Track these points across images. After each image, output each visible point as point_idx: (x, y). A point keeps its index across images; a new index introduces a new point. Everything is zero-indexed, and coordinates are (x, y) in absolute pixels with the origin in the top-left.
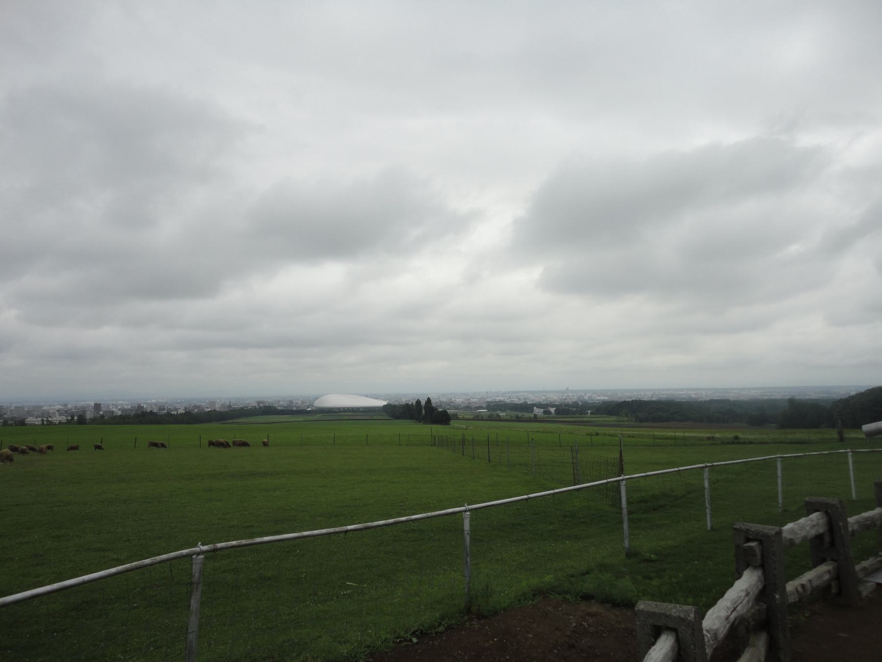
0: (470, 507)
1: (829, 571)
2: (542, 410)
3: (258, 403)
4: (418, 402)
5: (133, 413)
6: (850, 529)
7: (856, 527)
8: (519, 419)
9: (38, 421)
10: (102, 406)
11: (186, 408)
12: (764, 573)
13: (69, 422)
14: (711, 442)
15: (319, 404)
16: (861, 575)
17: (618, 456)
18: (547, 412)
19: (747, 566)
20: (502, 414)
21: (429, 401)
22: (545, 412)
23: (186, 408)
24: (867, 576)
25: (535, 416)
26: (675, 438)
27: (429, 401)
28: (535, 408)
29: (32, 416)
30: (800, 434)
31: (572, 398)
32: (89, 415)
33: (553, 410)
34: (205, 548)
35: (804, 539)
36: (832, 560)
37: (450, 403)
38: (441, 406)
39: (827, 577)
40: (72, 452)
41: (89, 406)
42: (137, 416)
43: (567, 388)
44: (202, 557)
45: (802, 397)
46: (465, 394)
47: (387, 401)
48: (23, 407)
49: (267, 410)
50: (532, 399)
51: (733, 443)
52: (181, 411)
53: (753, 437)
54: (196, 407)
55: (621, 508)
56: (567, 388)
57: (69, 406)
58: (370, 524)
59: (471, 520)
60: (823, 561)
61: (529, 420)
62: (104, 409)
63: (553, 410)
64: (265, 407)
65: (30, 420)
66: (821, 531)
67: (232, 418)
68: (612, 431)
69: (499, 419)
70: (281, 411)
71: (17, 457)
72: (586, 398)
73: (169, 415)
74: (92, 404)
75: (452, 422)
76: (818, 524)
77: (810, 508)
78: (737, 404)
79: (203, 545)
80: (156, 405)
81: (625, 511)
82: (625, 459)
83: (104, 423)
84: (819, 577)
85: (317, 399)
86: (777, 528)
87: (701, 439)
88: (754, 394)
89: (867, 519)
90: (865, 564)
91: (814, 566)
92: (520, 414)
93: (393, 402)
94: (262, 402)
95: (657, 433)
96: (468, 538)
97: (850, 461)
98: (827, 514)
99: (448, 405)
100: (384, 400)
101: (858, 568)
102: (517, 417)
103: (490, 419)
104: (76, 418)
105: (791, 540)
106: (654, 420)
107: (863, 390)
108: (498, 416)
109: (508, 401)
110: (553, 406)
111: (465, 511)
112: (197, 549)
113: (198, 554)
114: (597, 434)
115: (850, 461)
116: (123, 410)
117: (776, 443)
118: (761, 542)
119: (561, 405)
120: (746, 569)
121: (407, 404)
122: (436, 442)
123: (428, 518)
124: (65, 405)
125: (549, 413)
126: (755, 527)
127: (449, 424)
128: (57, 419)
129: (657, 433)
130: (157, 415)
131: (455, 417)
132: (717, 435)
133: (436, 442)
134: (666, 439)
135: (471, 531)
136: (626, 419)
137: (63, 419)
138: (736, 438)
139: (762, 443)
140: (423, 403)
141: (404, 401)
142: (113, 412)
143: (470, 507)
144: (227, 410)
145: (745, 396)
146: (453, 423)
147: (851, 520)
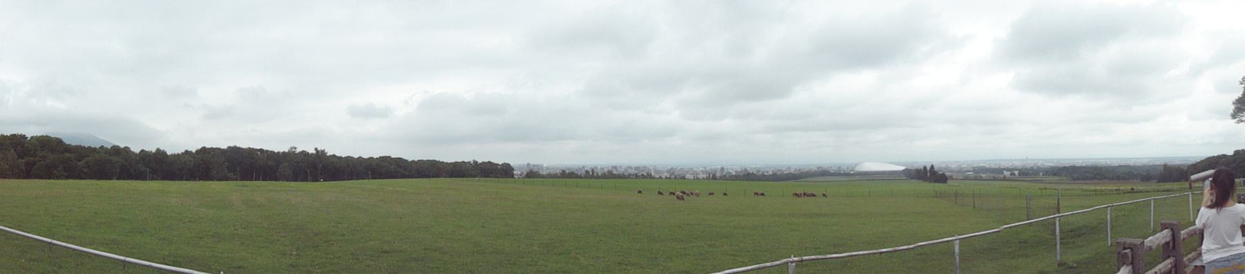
0: (959, 237)
1: (1171, 263)
2: (1009, 173)
3: (818, 168)
4: (925, 168)
5: (742, 174)
6: (1182, 238)
7: (1185, 236)
8: (995, 179)
9: (691, 177)
11: (773, 172)
12: (1133, 268)
13: (708, 178)
14: (1117, 192)
16: (1187, 263)
17: (1057, 202)
18: (1013, 174)
19: (1124, 264)
20: (983, 176)
21: (932, 167)
22: (1011, 174)
23: (773, 172)
24: (1190, 262)
25: (1005, 176)
26: (1096, 191)
27: (932, 167)
28: (1005, 171)
29: (688, 173)
30: (1168, 186)
31: (1030, 164)
32: (718, 175)
33: (1016, 173)
34: (796, 259)
35: (1158, 246)
36: (1173, 256)
37: (947, 168)
38: (940, 170)
39: (1170, 266)
40: (711, 196)
41: (718, 169)
42: (744, 176)
43: (1027, 158)
44: (794, 264)
45: (1171, 164)
46: (958, 162)
48: (683, 169)
49: (824, 173)
50: (1004, 165)
51: (1130, 192)
52: (771, 173)
53: (1141, 188)
54: (779, 170)
55: (1056, 236)
56: (1027, 158)
57: (708, 169)
58: (897, 248)
59: (960, 246)
60: (1169, 257)
61: (1001, 180)
62: (726, 171)
63: (1016, 173)
64: (823, 171)
65: (688, 176)
66: (1168, 240)
68: (1056, 186)
69: (981, 179)
71: (685, 196)
72: (1039, 164)
73: (763, 175)
74: (720, 167)
75: (949, 181)
76: (1166, 236)
77: (1164, 227)
78: (1134, 167)
79: (794, 257)
80: (755, 168)
81: (1058, 238)
82: (1061, 205)
83: (727, 180)
84: (1165, 267)
86: (1142, 240)
87: (1110, 190)
88: (1145, 162)
89: (1192, 230)
90: (1190, 256)
91: (1163, 261)
92: (996, 175)
93: (909, 167)
94: (821, 168)
95: (1085, 187)
96: (957, 257)
97: (1191, 199)
98: (1172, 229)
100: (903, 166)
101: (1185, 259)
102: (994, 177)
103: (975, 179)
104: (711, 176)
105: (1150, 247)
106: (1084, 179)
107: (1203, 159)
108: (981, 177)
109: (988, 166)
110: (1017, 170)
111: (956, 240)
112: (791, 260)
113: (792, 262)
114: (1046, 189)
115: (1191, 199)
116: (736, 172)
117: (1155, 191)
118: (1132, 249)
119: (1022, 169)
120: (1122, 266)
121: (918, 170)
122: (938, 195)
123: (930, 244)
124: (705, 168)
125: (1014, 174)
126: (1129, 240)
128: (701, 176)
129: (1085, 187)
131: (951, 178)
132: (1122, 188)
133: (938, 195)
134: (1090, 191)
135: (960, 254)
136: (1065, 178)
137: (705, 176)
138: (1132, 189)
139: (1147, 192)
140: (928, 168)
141: (916, 166)
142: (731, 173)
143: (959, 237)
144: (798, 172)
145: (1139, 163)
146: (950, 182)
147: (1183, 232)
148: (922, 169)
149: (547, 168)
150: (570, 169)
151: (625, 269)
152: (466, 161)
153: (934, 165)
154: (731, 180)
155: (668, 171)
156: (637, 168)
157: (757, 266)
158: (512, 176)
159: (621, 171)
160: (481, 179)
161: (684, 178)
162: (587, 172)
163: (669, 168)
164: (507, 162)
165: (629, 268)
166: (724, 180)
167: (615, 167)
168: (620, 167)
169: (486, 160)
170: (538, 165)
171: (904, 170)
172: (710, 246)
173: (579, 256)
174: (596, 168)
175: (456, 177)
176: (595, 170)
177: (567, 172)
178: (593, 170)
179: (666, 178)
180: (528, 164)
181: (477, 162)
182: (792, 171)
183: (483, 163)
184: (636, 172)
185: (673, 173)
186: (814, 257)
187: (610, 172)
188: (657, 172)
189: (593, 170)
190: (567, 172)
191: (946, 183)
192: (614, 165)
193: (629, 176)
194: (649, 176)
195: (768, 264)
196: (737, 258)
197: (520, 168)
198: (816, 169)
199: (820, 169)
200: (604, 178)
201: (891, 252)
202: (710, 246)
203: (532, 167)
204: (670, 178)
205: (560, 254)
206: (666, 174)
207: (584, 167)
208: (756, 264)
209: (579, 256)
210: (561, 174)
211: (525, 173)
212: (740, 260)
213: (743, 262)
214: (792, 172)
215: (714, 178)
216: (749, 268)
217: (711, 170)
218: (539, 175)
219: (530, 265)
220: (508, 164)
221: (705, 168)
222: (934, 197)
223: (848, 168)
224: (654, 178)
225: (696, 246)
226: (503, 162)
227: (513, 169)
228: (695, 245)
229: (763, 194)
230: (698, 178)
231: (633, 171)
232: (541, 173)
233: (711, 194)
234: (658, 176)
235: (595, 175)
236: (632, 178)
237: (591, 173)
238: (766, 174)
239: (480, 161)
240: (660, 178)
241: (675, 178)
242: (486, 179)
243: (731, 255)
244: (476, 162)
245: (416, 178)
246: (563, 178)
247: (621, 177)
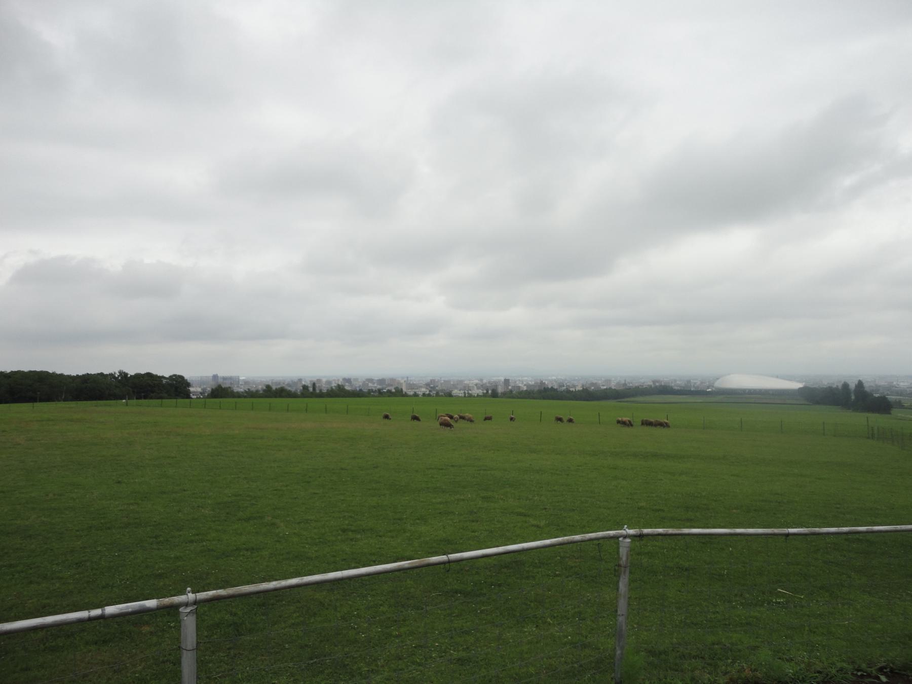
3: (654, 382)
5: (536, 389)
11: (583, 386)
13: (485, 395)
15: (720, 384)
29: (456, 388)
32: (500, 390)
34: (631, 532)
42: (540, 392)
47: (804, 384)
49: (663, 390)
52: (579, 388)
54: (593, 384)
57: (485, 381)
58: (817, 530)
62: (512, 384)
65: (455, 392)
67: (623, 397)
70: (678, 391)
73: (568, 391)
74: (502, 379)
79: (629, 528)
80: (555, 381)
83: (513, 397)
85: (718, 379)
94: (658, 381)
99: (889, 390)
104: (490, 392)
113: (625, 537)
122: (872, 435)
124: (481, 380)
127: (890, 414)
128: (476, 392)
130: (557, 391)
131: (900, 405)
137: (480, 392)
144: (622, 388)
146: (895, 412)
148: (840, 387)
149: (246, 382)
150: (279, 384)
152: (106, 372)
155: (427, 385)
156: (382, 381)
158: (187, 395)
159: (357, 385)
160: (131, 402)
161: (449, 395)
162: (305, 387)
163: (428, 379)
164: (178, 373)
165: (359, 536)
166: (509, 397)
167: (348, 380)
168: (356, 380)
169: (143, 371)
170: (231, 378)
171: (800, 389)
174: (319, 380)
175: (86, 399)
176: (317, 385)
177: (274, 388)
178: (314, 385)
179: (424, 395)
180: (215, 377)
181: (126, 374)
182: (613, 385)
183: (138, 376)
184: (379, 387)
185: (434, 388)
188: (411, 386)
189: (314, 385)
190: (274, 388)
193: (369, 394)
194: (399, 393)
197: (201, 382)
198: (651, 383)
199: (657, 384)
201: (805, 535)
203: (220, 381)
204: (429, 395)
205: (248, 520)
206: (423, 390)
207: (300, 380)
210: (264, 391)
212: (535, 522)
214: (613, 388)
215: (495, 394)
218: (232, 392)
219: (192, 542)
220: (182, 377)
221: (481, 380)
224: (406, 395)
225: (463, 500)
227: (188, 385)
228: (462, 497)
229: (570, 421)
230: (470, 396)
231: (375, 385)
232: (236, 389)
234: (412, 393)
236: (374, 396)
237: (311, 389)
238: (571, 389)
239: (131, 372)
240: (416, 395)
241: (437, 394)
243: (520, 514)
244: (124, 375)
245: (6, 402)
246: (266, 397)
247: (357, 394)
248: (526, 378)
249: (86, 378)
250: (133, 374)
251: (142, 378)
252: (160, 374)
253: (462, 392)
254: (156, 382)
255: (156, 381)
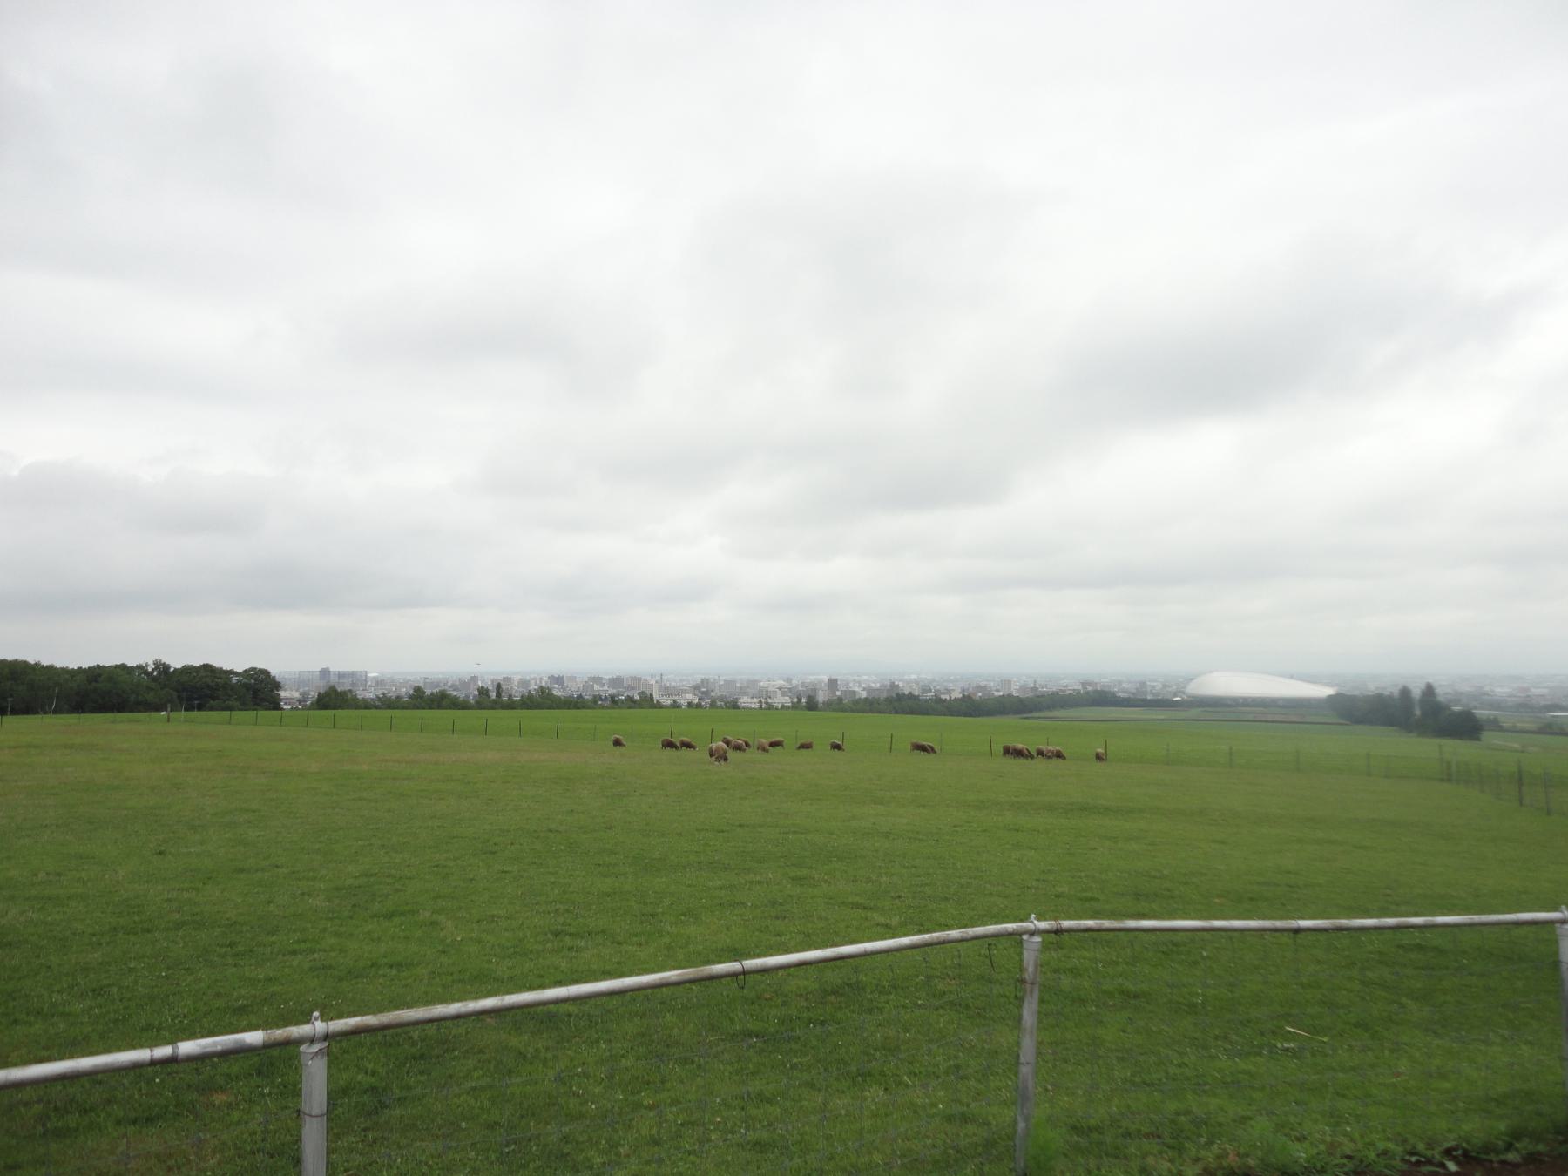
3: (1084, 684)
5: (884, 696)
9: (753, 703)
10: (839, 683)
11: (963, 690)
13: (795, 706)
29: (746, 694)
34: (1043, 925)
40: (804, 751)
42: (889, 700)
44: (1037, 939)
48: (734, 682)
49: (1100, 698)
52: (957, 695)
54: (979, 688)
57: (794, 682)
65: (744, 701)
71: (731, 754)
73: (938, 700)
74: (825, 679)
79: (1039, 920)
80: (917, 682)
83: (843, 710)
85: (1192, 679)
93: (1348, 691)
94: (1090, 684)
100: (1329, 685)
104: (804, 700)
113: (1032, 933)
116: (869, 690)
122: (1449, 775)
124: (789, 680)
128: (779, 700)
130: (919, 700)
131: (1495, 725)
137: (787, 701)
142: (854, 692)
144: (1030, 695)
146: (1488, 737)
149: (379, 683)
151: (570, 949)
152: (131, 663)
153: (1435, 685)
154: (858, 711)
155: (696, 688)
156: (617, 681)
157: (926, 937)
158: (275, 705)
159: (574, 689)
160: (174, 715)
161: (735, 706)
162: (483, 692)
163: (697, 679)
167: (559, 680)
168: (572, 678)
170: (352, 675)
171: (1330, 697)
172: (798, 880)
173: (442, 918)
174: (508, 679)
176: (504, 687)
177: (428, 692)
178: (499, 687)
179: (690, 705)
180: (325, 672)
181: (166, 667)
183: (187, 670)
184: (612, 691)
186: (1090, 923)
187: (544, 693)
188: (668, 690)
189: (499, 687)
190: (428, 692)
191: (1478, 739)
192: (556, 673)
193: (595, 702)
194: (647, 702)
195: (954, 934)
196: (869, 914)
197: (299, 682)
199: (1090, 688)
200: (529, 707)
202: (798, 880)
203: (333, 680)
204: (699, 706)
205: (390, 916)
206: (689, 696)
207: (474, 679)
208: (920, 932)
209: (442, 918)
210: (411, 697)
211: (314, 694)
213: (887, 926)
215: (812, 705)
216: (905, 941)
217: (803, 684)
218: (355, 698)
219: (294, 953)
220: (266, 673)
222: (1442, 780)
223: (1165, 686)
224: (659, 706)
225: (760, 883)
226: (247, 667)
227: (277, 686)
228: (758, 878)
230: (770, 707)
231: (606, 688)
233: (806, 746)
235: (505, 698)
236: (603, 707)
237: (493, 695)
238: (943, 697)
239: (176, 663)
240: (675, 705)
241: (713, 705)
242: (195, 714)
243: (857, 906)
244: (163, 668)
247: (574, 703)
248: (865, 677)
249: (95, 674)
250: (179, 666)
251: (195, 674)
252: (227, 667)
253: (756, 700)
254: (219, 680)
255: (221, 678)
